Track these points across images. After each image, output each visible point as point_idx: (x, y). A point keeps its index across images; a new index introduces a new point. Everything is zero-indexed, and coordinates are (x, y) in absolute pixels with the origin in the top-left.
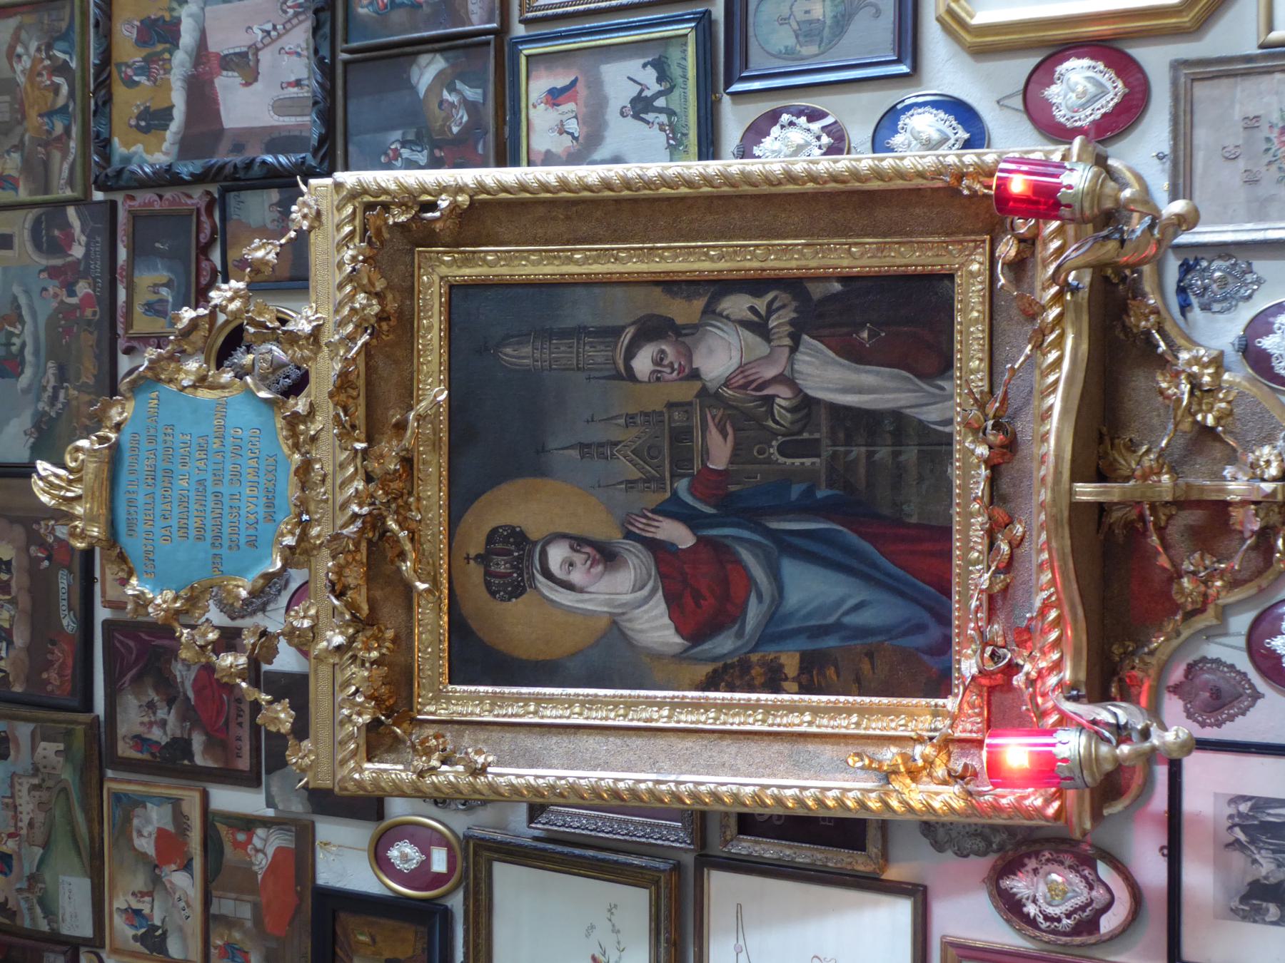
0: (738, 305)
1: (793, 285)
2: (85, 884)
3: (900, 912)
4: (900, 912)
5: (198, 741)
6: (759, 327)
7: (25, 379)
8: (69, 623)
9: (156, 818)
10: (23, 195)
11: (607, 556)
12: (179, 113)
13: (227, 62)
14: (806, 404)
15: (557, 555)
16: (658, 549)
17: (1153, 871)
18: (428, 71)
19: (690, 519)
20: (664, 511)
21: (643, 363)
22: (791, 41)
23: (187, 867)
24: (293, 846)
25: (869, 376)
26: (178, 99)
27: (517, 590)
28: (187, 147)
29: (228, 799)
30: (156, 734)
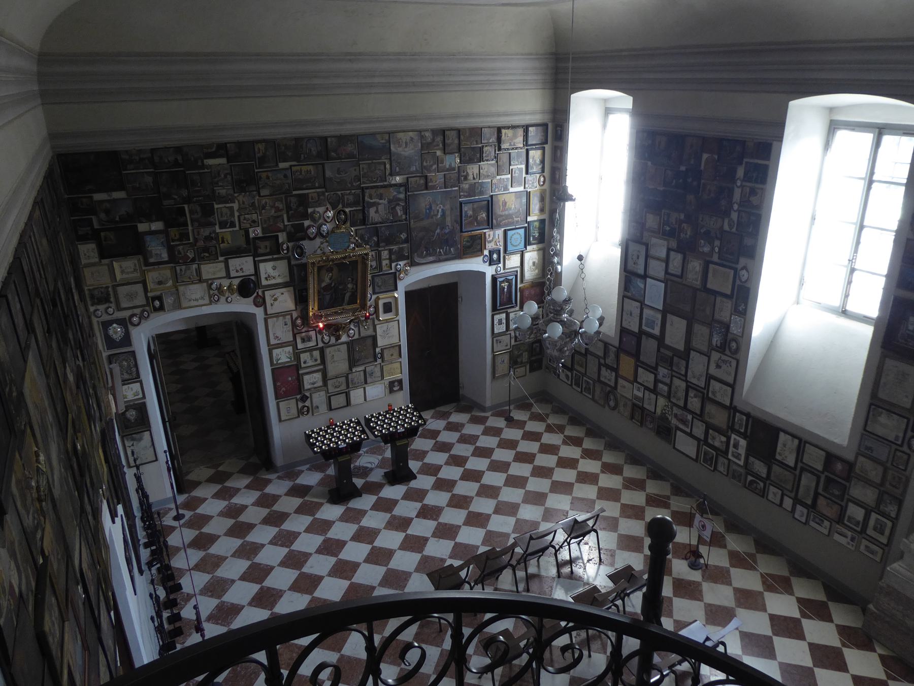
0: (355, 287)
1: (356, 291)
2: (268, 194)
3: (294, 309)
4: (294, 309)
5: (292, 212)
6: (353, 288)
7: (337, 175)
8: (304, 186)
9: (281, 206)
10: (361, 173)
11: (330, 279)
12: (372, 201)
13: (377, 208)
14: (345, 294)
15: (331, 274)
16: (331, 284)
17: (303, 330)
18: (375, 239)
19: (334, 286)
20: (335, 284)
21: (349, 279)
22: (706, 586)
23: (275, 212)
24: (452, 614)
25: (348, 299)
26: (373, 201)
27: (327, 271)
28: (368, 202)
29: (285, 216)
30: (292, 204)
